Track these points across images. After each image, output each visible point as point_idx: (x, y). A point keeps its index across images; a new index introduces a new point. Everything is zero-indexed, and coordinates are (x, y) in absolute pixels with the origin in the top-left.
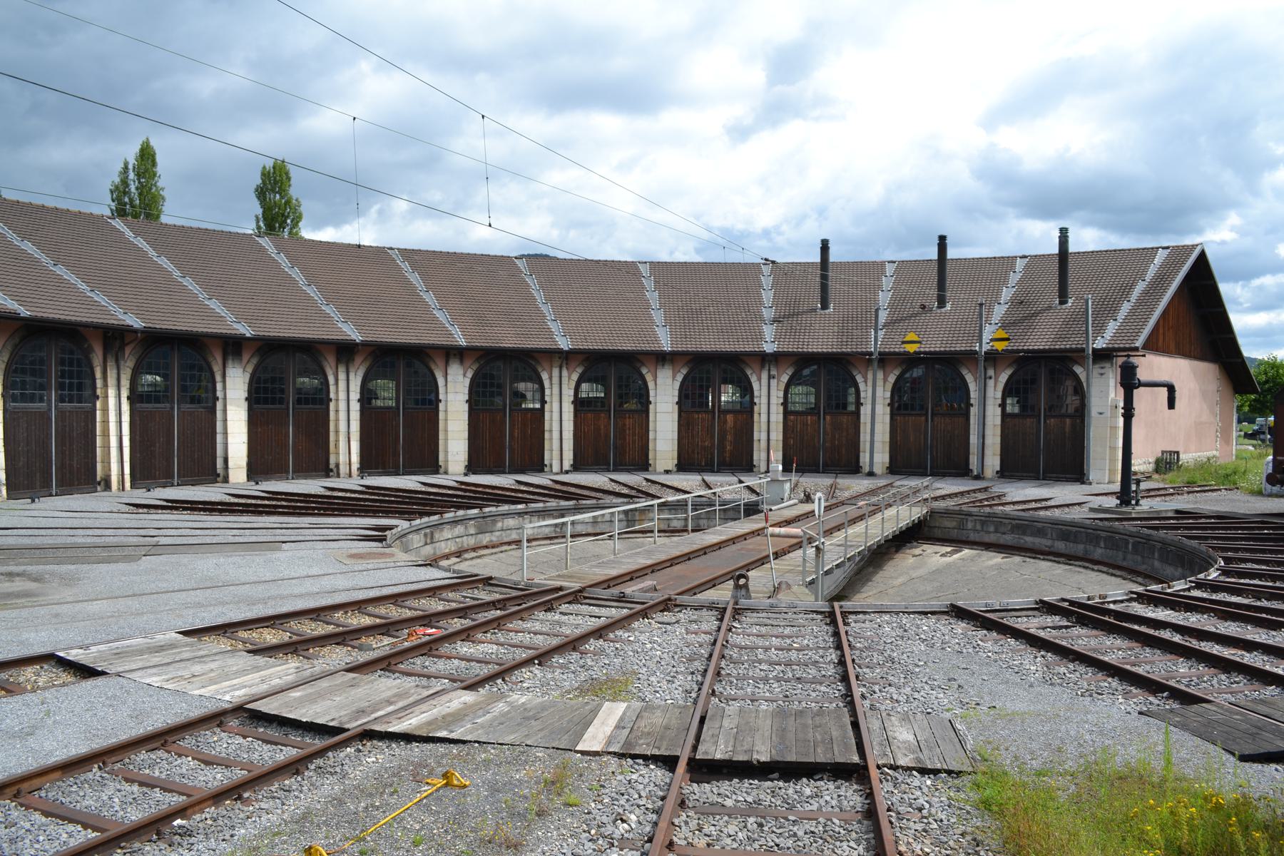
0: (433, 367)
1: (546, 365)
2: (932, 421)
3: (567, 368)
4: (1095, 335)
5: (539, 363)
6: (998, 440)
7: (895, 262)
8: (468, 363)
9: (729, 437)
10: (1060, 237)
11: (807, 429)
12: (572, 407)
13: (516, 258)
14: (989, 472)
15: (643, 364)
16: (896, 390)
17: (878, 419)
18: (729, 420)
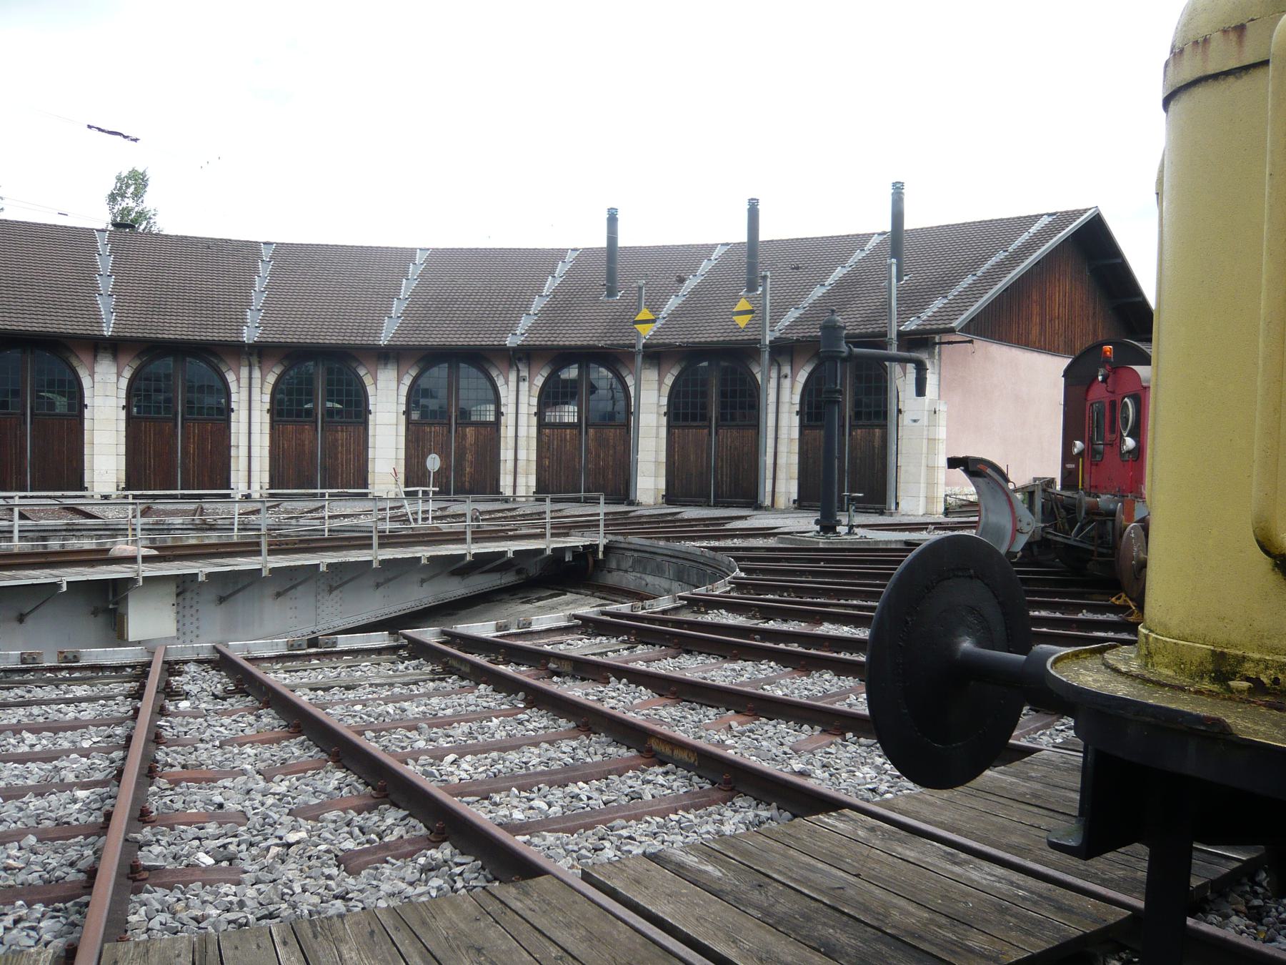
0: (75, 363)
1: (86, 358)
2: (456, 431)
3: (260, 368)
4: (772, 321)
5: (222, 360)
6: (795, 459)
7: (272, 244)
8: (124, 359)
9: (469, 457)
10: (893, 194)
11: (565, 447)
12: (267, 418)
13: (97, 230)
14: (782, 502)
15: (361, 363)
16: (675, 395)
17: (256, 428)
18: (469, 435)
